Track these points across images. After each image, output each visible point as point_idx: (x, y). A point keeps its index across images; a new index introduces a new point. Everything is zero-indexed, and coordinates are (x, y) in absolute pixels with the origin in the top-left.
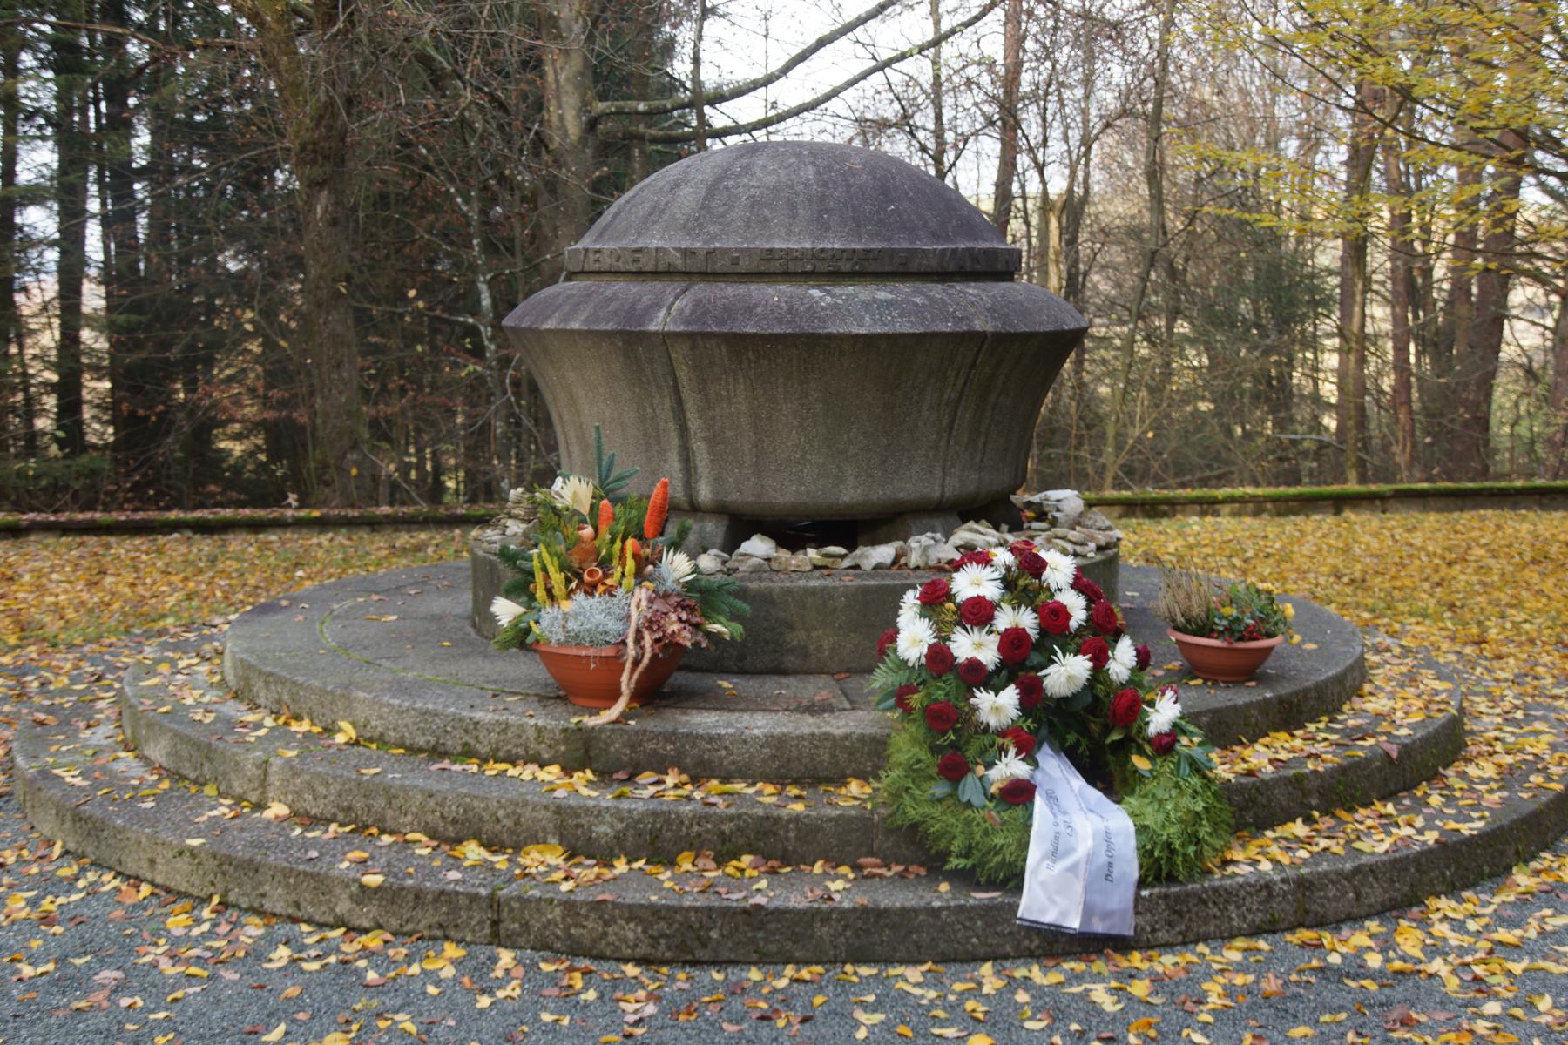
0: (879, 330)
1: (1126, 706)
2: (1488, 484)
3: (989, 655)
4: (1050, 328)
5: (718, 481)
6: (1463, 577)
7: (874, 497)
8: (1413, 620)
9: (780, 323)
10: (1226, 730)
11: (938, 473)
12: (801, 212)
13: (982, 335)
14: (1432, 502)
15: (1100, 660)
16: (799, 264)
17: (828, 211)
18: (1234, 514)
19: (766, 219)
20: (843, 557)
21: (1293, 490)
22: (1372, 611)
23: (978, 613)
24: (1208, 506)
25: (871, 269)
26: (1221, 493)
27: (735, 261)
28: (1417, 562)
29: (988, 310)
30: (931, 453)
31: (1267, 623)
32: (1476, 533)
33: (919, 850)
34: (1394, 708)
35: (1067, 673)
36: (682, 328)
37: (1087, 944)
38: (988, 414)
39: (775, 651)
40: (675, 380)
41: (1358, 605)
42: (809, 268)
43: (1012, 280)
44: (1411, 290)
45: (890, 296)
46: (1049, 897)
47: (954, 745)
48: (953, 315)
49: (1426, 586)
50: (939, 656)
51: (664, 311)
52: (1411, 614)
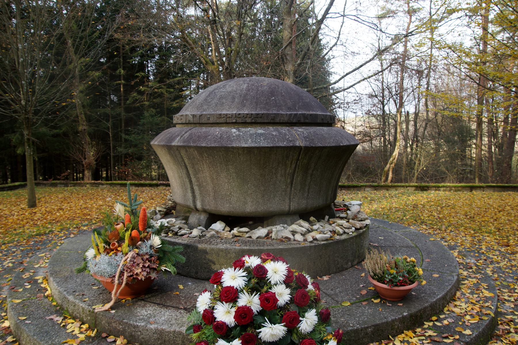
0: (253, 145)
2: (511, 185)
4: (333, 145)
5: (203, 201)
6: (503, 217)
7: (259, 210)
8: (487, 235)
9: (215, 142)
11: (287, 201)
12: (236, 100)
13: (300, 148)
14: (496, 189)
16: (231, 119)
17: (246, 100)
18: (444, 191)
19: (223, 103)
20: (247, 232)
21: (460, 185)
22: (474, 230)
24: (437, 188)
25: (259, 121)
26: (441, 185)
27: (209, 119)
28: (490, 211)
29: (304, 138)
30: (283, 193)
31: (411, 277)
32: (507, 201)
36: (182, 144)
38: (309, 178)
39: (208, 272)
40: (185, 164)
41: (470, 228)
42: (234, 121)
43: (331, 126)
44: (493, 134)
45: (263, 132)
48: (288, 139)
49: (492, 220)
51: (179, 137)
52: (486, 232)
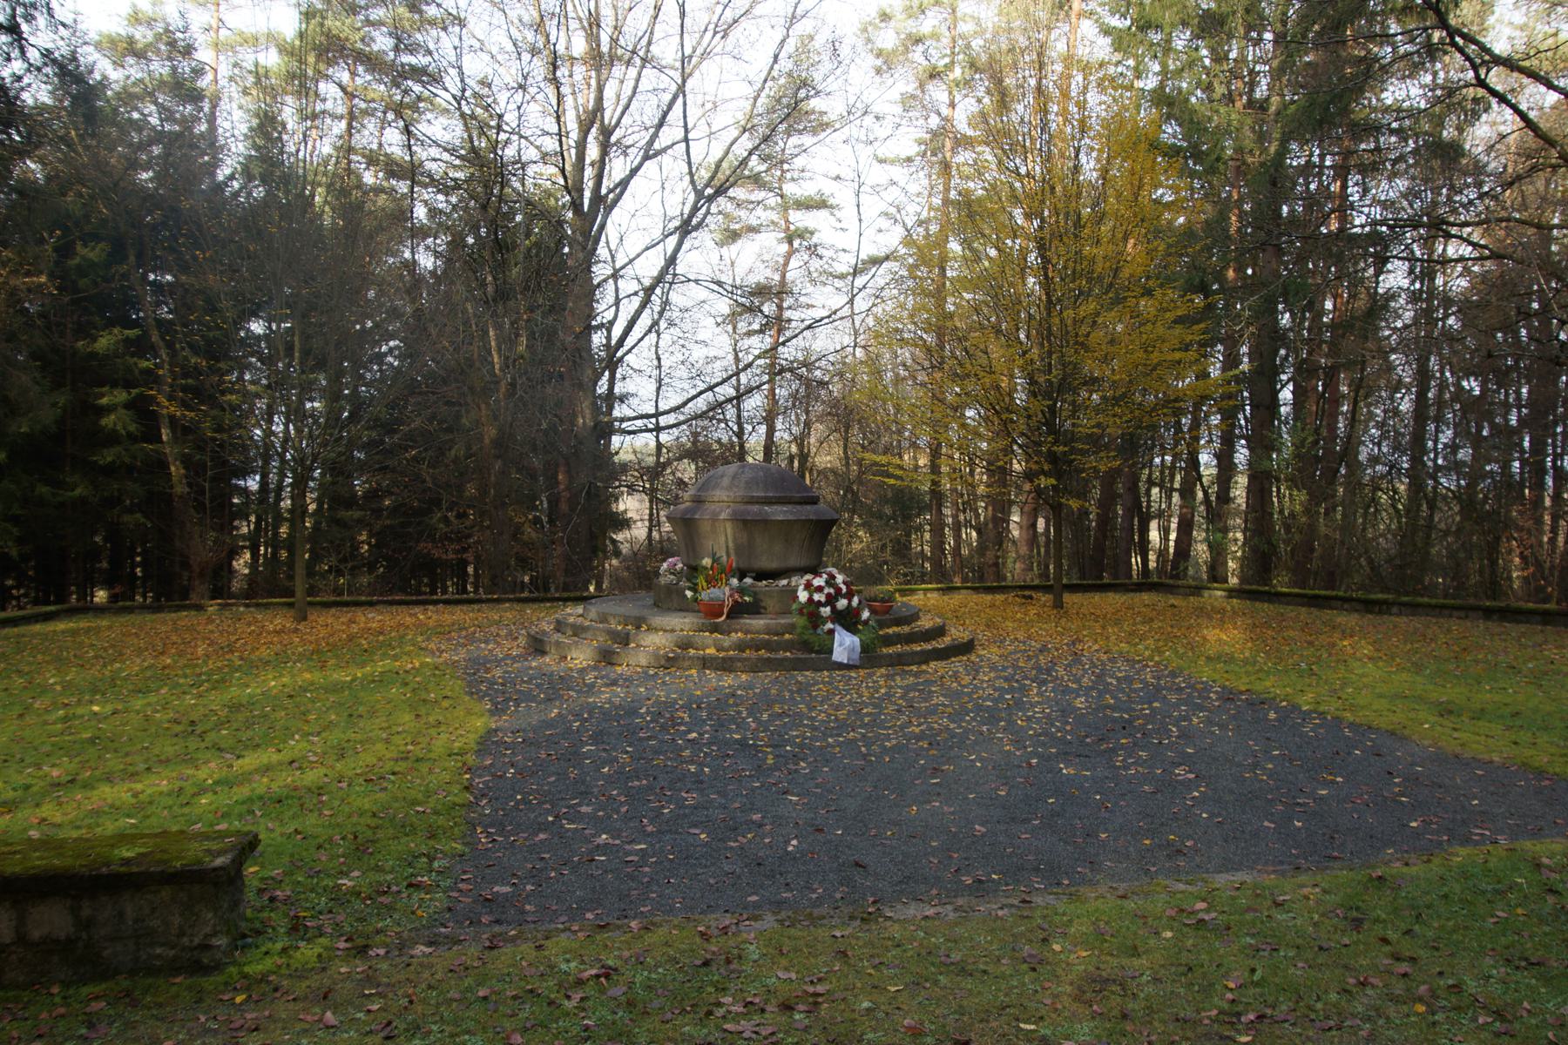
1: (857, 612)
3: (823, 599)
10: (882, 625)
15: (850, 601)
23: (820, 589)
33: (806, 646)
34: (926, 623)
35: (842, 603)
37: (848, 667)
46: (839, 655)
47: (814, 619)
50: (810, 600)
